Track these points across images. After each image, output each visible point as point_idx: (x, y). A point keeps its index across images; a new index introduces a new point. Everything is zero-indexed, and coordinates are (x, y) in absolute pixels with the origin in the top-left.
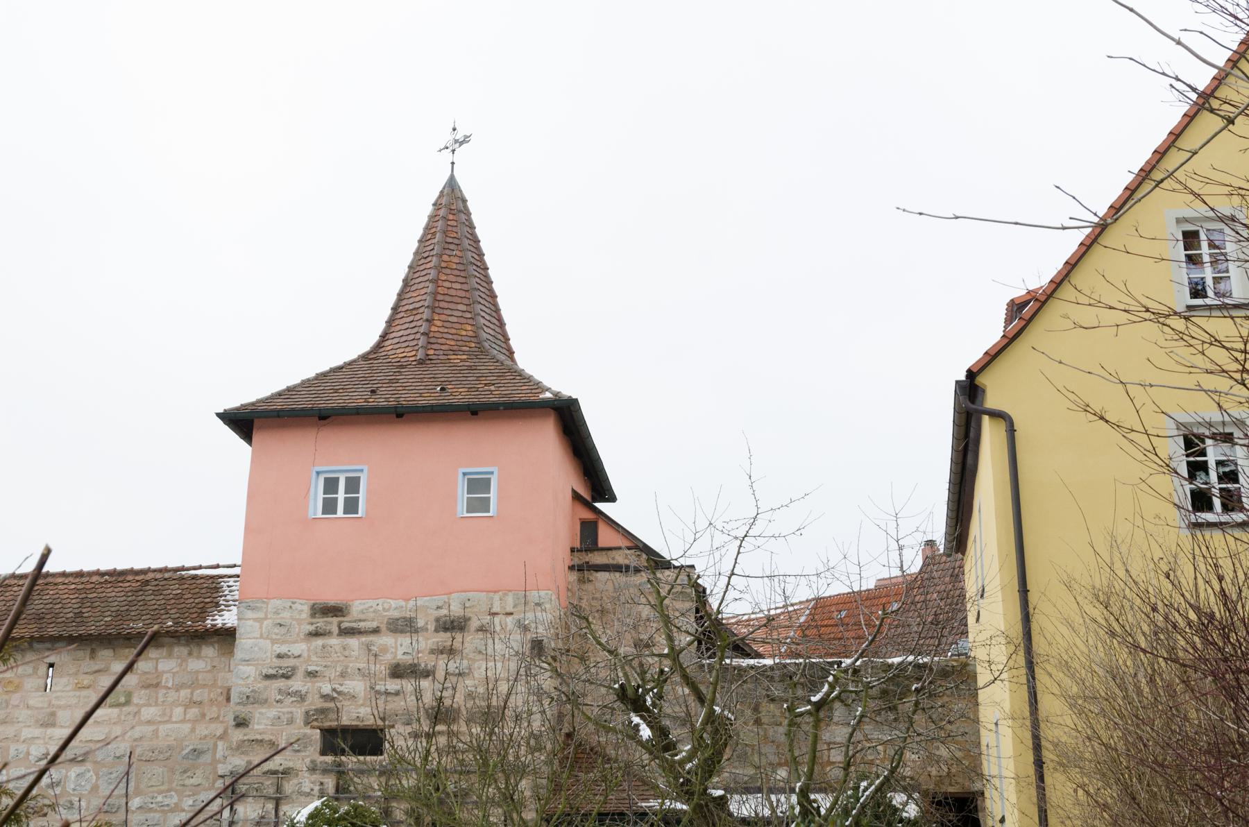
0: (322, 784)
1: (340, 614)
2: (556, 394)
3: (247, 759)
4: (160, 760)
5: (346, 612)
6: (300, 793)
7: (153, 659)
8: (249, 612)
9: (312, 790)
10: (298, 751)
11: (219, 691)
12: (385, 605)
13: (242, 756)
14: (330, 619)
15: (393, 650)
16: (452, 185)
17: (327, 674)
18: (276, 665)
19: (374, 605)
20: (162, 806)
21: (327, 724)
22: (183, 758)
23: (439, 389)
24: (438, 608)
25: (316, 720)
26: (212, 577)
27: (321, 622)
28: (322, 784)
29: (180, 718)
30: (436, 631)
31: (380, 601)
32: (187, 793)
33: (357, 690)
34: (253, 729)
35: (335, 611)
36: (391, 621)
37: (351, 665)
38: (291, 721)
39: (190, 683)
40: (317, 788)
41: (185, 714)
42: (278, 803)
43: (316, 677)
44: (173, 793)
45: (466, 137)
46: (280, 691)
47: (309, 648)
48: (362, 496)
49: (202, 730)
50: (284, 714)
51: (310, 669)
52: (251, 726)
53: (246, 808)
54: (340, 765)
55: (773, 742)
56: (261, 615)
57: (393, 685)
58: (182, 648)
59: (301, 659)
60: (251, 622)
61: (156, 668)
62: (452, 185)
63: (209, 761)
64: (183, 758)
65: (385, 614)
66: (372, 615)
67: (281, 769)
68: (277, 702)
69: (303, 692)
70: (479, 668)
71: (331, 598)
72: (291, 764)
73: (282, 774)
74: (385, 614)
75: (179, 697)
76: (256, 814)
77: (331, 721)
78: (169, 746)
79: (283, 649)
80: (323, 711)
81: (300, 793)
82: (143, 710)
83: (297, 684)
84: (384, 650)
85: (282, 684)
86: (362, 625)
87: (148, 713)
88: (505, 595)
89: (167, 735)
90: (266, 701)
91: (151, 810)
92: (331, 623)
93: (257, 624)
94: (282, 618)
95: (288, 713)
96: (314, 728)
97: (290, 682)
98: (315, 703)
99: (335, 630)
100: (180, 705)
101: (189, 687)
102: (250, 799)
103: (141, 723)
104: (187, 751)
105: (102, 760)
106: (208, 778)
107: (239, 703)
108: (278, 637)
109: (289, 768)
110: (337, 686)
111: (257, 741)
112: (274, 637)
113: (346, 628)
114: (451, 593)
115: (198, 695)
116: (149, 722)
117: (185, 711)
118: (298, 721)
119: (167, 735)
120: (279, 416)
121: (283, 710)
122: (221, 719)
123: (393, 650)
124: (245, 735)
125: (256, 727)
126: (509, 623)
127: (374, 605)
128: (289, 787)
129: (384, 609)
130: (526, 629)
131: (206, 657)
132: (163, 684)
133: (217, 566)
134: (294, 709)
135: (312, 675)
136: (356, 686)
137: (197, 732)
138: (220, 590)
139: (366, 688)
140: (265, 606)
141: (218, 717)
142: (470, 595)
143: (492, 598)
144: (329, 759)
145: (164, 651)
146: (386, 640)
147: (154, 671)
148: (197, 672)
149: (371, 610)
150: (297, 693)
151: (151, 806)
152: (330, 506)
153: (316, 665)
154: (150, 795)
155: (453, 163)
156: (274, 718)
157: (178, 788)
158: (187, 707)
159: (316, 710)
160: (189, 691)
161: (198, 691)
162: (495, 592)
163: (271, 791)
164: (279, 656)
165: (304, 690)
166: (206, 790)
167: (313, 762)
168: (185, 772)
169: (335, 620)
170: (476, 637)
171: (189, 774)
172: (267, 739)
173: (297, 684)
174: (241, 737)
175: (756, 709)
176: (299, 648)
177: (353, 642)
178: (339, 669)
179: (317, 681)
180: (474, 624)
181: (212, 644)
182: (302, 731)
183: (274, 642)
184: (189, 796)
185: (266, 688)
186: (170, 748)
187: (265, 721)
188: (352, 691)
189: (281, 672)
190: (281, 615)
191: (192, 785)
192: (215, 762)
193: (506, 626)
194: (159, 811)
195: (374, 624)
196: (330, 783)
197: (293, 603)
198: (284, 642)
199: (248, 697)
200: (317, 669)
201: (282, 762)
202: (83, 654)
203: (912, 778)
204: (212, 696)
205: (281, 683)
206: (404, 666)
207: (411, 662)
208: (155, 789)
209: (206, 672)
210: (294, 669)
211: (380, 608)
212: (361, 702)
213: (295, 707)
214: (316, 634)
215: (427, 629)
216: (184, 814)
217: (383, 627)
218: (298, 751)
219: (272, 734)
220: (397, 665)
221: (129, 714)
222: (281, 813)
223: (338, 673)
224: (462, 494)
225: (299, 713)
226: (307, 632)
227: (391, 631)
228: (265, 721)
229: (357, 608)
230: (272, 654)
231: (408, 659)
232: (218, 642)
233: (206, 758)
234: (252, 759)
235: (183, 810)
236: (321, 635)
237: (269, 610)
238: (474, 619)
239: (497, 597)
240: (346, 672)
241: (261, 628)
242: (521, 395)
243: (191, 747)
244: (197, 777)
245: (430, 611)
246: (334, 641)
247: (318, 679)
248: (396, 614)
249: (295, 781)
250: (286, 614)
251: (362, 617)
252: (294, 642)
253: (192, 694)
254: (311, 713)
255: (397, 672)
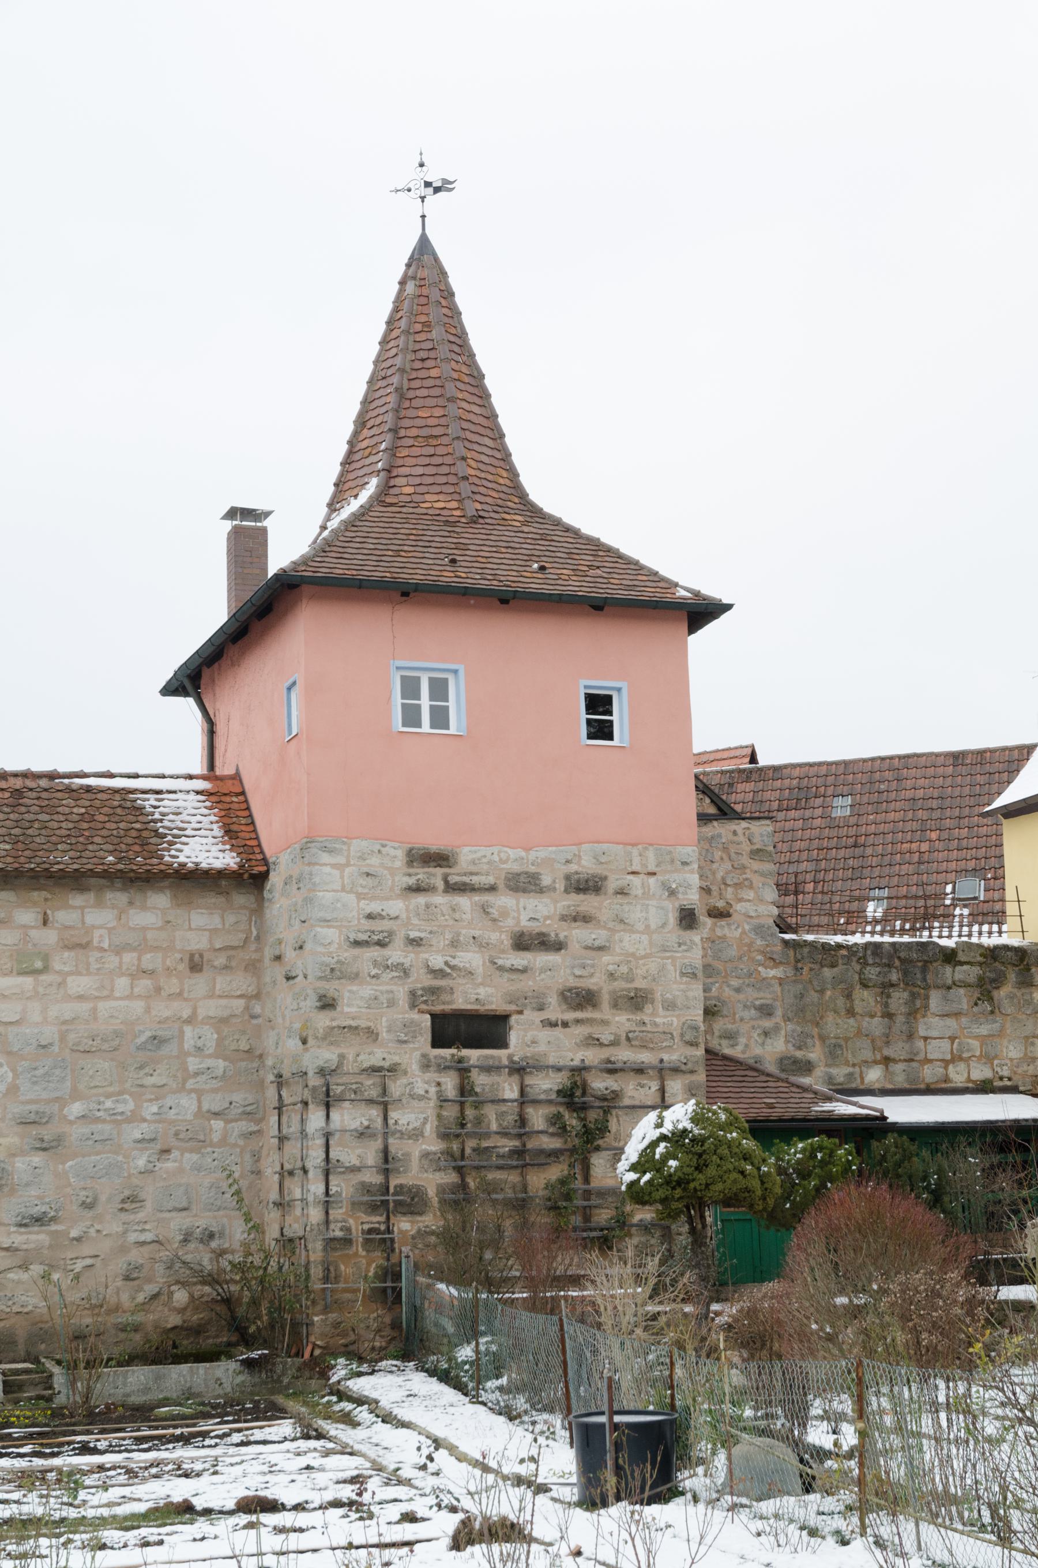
0: (439, 1084)
1: (445, 863)
2: (697, 594)
3: (338, 1051)
4: (105, 1051)
5: (452, 860)
6: (412, 1096)
7: (75, 908)
8: (325, 855)
9: (427, 1092)
10: (405, 1042)
11: (178, 956)
12: (502, 855)
13: (332, 1047)
14: (431, 870)
15: (516, 915)
16: (424, 246)
17: (434, 942)
18: (366, 928)
19: (488, 854)
20: (114, 1114)
21: (438, 1008)
22: (138, 1048)
23: (536, 566)
24: (568, 862)
25: (425, 1002)
26: (116, 791)
27: (421, 874)
28: (439, 1084)
29: (127, 993)
30: (566, 891)
31: (495, 849)
32: (149, 1096)
33: (474, 964)
34: (342, 1012)
35: (439, 859)
36: (510, 876)
37: (464, 931)
38: (392, 1003)
39: (137, 943)
40: (433, 1090)
41: (132, 988)
42: (385, 1107)
43: (420, 945)
44: (127, 1097)
45: (446, 181)
46: (375, 963)
47: (407, 907)
48: (398, 701)
49: (163, 1009)
50: (382, 992)
51: (413, 934)
52: (339, 1009)
53: (342, 1115)
54: (460, 1061)
55: (867, 1035)
56: (341, 860)
57: (519, 959)
58: (118, 894)
59: (399, 922)
60: (327, 869)
61: (83, 923)
62: (424, 246)
63: (175, 1053)
64: (138, 1048)
65: (503, 866)
66: (485, 867)
67: (386, 1064)
68: (374, 977)
69: (406, 965)
70: (621, 941)
71: (434, 843)
72: (396, 1059)
73: (389, 1071)
74: (503, 866)
75: (121, 963)
76: (358, 1123)
77: (444, 1003)
78: (115, 1032)
79: (374, 907)
80: (433, 991)
81: (412, 1096)
82: (70, 979)
83: (396, 954)
84: (504, 913)
85: (376, 954)
86: (475, 880)
87: (78, 984)
88: (646, 849)
89: (112, 1017)
90: (357, 975)
91: (97, 1120)
92: (434, 875)
93: (336, 873)
94: (368, 865)
95: (388, 992)
96: (423, 1012)
97: (386, 952)
98: (421, 980)
99: (440, 885)
100: (123, 975)
101: (134, 949)
102: (347, 1104)
103: (69, 998)
104: (143, 1038)
105: (20, 1050)
106: (175, 1076)
107: (320, 978)
108: (366, 891)
109: (396, 1064)
110: (449, 959)
111: (350, 1027)
112: (360, 890)
113: (456, 883)
114: (580, 844)
115: (149, 960)
116: (81, 998)
117: (132, 984)
118: (401, 1002)
119: (112, 1017)
120: (360, 587)
121: (380, 988)
122: (186, 995)
123: (516, 915)
124: (333, 1020)
125: (346, 1009)
126: (652, 886)
127: (488, 854)
128: (396, 1088)
129: (501, 860)
130: (672, 893)
131: (154, 908)
132: (95, 944)
133: (136, 776)
134: (394, 988)
135: (415, 943)
136: (471, 959)
137: (154, 1013)
138: (223, 813)
139: (484, 962)
140: (345, 847)
141: (180, 994)
142: (605, 846)
143: (631, 853)
144: (446, 1053)
145: (91, 896)
146: (504, 901)
147: (80, 925)
148: (144, 929)
149: (484, 860)
150: (398, 966)
151: (99, 1114)
152: (412, 717)
153: (419, 930)
154: (94, 1099)
155: (423, 217)
156: (370, 999)
157: (133, 1090)
158: (133, 977)
159: (423, 989)
160: (135, 955)
161: (148, 956)
162: (634, 845)
163: (374, 1093)
164: (370, 917)
165: (407, 962)
166: (174, 1092)
167: (424, 1056)
168: (141, 1068)
169: (439, 872)
170: (615, 901)
171: (147, 1070)
172: (363, 1026)
173: (396, 954)
174: (328, 1023)
175: (849, 996)
176: (396, 907)
177: (464, 901)
178: (448, 936)
179: (421, 952)
180: (612, 885)
181: (161, 890)
182: (407, 1016)
183: (360, 897)
184: (151, 1100)
185: (355, 958)
186: (117, 1034)
187: (358, 1002)
188: (468, 965)
189: (376, 938)
190: (368, 861)
191: (154, 1086)
192: (183, 1054)
193: (649, 890)
194: (110, 1122)
195: (491, 880)
196: (450, 1083)
197: (384, 846)
198: (374, 898)
199: (332, 970)
200: (422, 935)
201: (385, 1055)
202: (118, 898)
203: (1010, 1079)
204: (168, 962)
205: (375, 952)
206: (530, 934)
207: (537, 930)
208: (100, 1090)
209: (157, 929)
210: (391, 934)
211: (496, 858)
212: (480, 980)
213: (396, 984)
214: (417, 889)
215: (555, 889)
216: (145, 1125)
217: (501, 885)
218: (405, 1042)
219: (368, 1019)
220: (522, 934)
221: (51, 985)
222: (391, 1122)
223: (447, 942)
224: (619, 717)
225: (401, 993)
226: (404, 886)
227: (511, 889)
228: (358, 1002)
229: (466, 856)
230: (359, 914)
231: (536, 927)
232: (170, 887)
233: (167, 1050)
234: (345, 1051)
235: (145, 1120)
236: (424, 890)
237: (352, 853)
238: (612, 877)
239: (635, 852)
240: (458, 941)
241: (342, 877)
242: (648, 593)
243: (148, 1034)
244: (160, 1075)
245: (557, 866)
246: (440, 899)
247: (422, 948)
248: (516, 868)
249: (404, 1081)
250: (374, 861)
251: (472, 868)
252: (387, 899)
253: (139, 959)
254: (420, 992)
255: (522, 942)
